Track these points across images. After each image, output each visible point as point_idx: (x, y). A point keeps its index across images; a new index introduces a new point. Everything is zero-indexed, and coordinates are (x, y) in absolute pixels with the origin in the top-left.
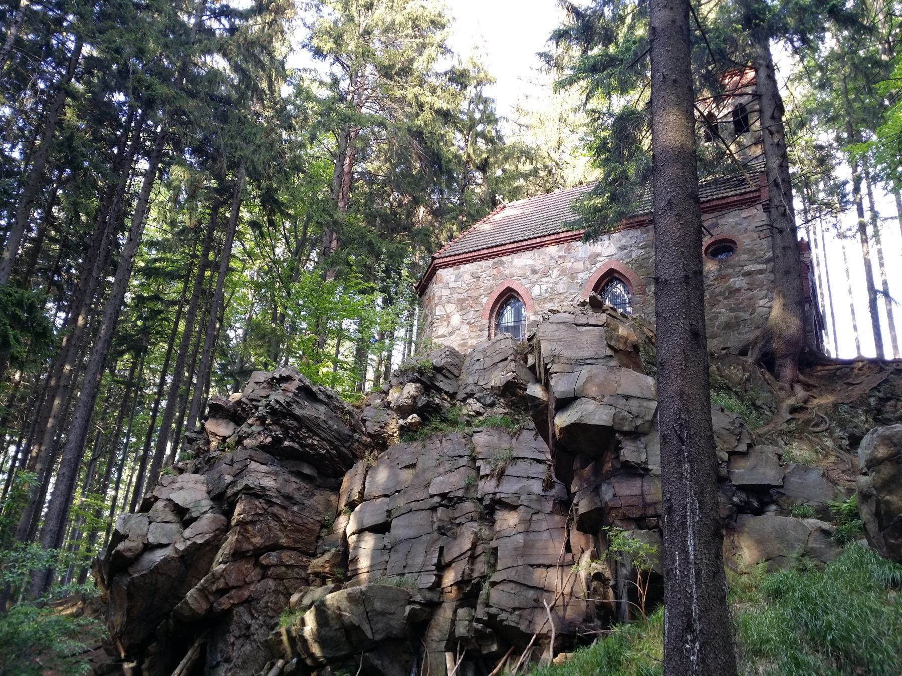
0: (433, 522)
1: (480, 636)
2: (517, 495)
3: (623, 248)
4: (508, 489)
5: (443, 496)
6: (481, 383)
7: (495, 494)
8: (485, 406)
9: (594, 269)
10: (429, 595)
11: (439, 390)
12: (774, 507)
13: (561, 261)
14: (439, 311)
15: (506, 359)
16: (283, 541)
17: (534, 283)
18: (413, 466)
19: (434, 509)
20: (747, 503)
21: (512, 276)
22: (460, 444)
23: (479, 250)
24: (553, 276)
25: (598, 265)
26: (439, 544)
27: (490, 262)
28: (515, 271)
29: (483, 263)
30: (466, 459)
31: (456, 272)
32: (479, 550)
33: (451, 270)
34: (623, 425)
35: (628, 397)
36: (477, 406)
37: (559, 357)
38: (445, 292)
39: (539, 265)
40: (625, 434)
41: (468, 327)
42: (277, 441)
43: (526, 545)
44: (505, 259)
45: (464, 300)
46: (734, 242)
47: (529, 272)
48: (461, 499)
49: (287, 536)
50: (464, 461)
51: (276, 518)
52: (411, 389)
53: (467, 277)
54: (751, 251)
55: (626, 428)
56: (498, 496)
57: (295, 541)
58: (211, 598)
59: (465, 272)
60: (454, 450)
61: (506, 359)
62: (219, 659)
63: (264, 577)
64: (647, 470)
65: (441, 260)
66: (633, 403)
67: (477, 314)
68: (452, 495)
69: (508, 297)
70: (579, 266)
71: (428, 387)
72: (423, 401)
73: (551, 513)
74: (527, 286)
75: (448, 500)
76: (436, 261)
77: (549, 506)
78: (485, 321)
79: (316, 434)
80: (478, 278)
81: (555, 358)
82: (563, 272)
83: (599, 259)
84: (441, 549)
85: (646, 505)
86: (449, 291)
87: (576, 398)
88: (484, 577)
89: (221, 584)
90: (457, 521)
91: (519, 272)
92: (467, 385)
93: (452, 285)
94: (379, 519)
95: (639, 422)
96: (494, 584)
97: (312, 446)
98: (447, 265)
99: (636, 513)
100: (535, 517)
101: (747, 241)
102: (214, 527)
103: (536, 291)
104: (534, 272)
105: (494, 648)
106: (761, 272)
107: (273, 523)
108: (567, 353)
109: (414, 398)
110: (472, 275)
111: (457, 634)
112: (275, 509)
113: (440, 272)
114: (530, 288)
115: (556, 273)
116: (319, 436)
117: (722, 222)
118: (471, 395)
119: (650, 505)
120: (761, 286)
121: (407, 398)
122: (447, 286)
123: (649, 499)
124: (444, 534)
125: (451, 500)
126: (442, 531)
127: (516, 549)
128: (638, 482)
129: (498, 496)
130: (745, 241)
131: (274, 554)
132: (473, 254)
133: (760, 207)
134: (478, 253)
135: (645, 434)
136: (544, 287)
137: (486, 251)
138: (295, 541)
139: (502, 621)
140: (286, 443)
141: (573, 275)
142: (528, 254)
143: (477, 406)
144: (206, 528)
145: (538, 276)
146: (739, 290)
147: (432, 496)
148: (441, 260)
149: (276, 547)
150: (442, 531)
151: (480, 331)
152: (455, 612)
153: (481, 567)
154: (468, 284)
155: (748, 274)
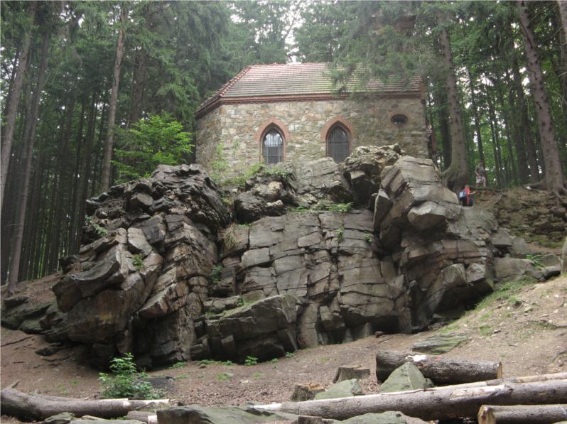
0: (302, 262)
1: (336, 319)
2: (353, 247)
3: (345, 110)
4: (346, 246)
5: (306, 248)
6: (314, 185)
7: (339, 247)
8: (317, 198)
9: (328, 120)
10: (304, 300)
11: (291, 187)
12: (508, 255)
13: (307, 112)
14: (224, 132)
15: (332, 173)
16: (199, 271)
17: (290, 123)
18: (281, 230)
19: (302, 255)
20: (498, 252)
21: (274, 116)
22: (312, 219)
23: (252, 97)
24: (302, 120)
25: (330, 118)
26: (307, 273)
27: (260, 106)
28: (277, 113)
29: (255, 105)
30: (317, 227)
31: (235, 108)
32: (333, 276)
33: (231, 106)
34: (448, 215)
35: (449, 202)
36: (313, 198)
37: (412, 179)
38: (228, 121)
39: (293, 111)
40: (448, 220)
41: (245, 145)
42: (195, 211)
43: (360, 274)
44: (269, 104)
45: (242, 127)
46: (406, 118)
47: (286, 115)
48: (317, 250)
49: (201, 268)
50: (316, 229)
51: (197, 257)
52: (277, 185)
53: (243, 112)
54: (415, 124)
55: (450, 217)
56: (341, 248)
57: (205, 271)
58: (170, 303)
59: (241, 109)
60: (308, 222)
61: (332, 173)
62: (169, 338)
63: (190, 291)
64: (460, 237)
65: (225, 99)
66: (451, 205)
67: (252, 137)
68: (312, 247)
69: (273, 129)
70: (318, 116)
71: (285, 185)
72: (284, 193)
73: (372, 258)
74: (286, 124)
75: (310, 250)
76: (221, 99)
77: (370, 254)
78: (257, 142)
79: (213, 208)
80: (251, 114)
81: (411, 179)
82: (309, 119)
83: (331, 114)
84: (309, 276)
85: (458, 253)
86: (230, 120)
87: (425, 201)
88: (337, 290)
89: (174, 295)
90: (317, 261)
91: (280, 114)
92: (304, 186)
93: (233, 116)
94: (267, 259)
95: (454, 215)
96: (343, 294)
97: (211, 215)
98: (229, 103)
99: (453, 256)
100: (364, 260)
101: (413, 118)
102: (157, 262)
103: (291, 127)
104: (290, 116)
105: (343, 325)
106: (420, 136)
107: (195, 261)
108: (416, 178)
109: (278, 191)
110: (247, 112)
111: (323, 319)
112: (197, 252)
113: (224, 107)
114: (288, 125)
115: (303, 119)
116: (215, 209)
117: (399, 104)
118: (308, 191)
119: (460, 253)
120: (420, 143)
121: (273, 190)
122: (229, 116)
123: (460, 250)
124: (309, 268)
125: (311, 250)
126: (308, 267)
127: (355, 276)
128: (455, 243)
129: (341, 248)
130: (411, 117)
131: (195, 278)
132: (248, 98)
133: (420, 100)
134: (251, 98)
135: (457, 220)
136: (297, 126)
137: (257, 98)
138: (205, 271)
139: (352, 311)
140: (200, 213)
141: (315, 121)
142: (287, 104)
143: (313, 198)
144: (153, 262)
145: (292, 119)
146: (409, 144)
147: (300, 248)
148: (225, 99)
149: (196, 275)
150: (308, 267)
151: (254, 148)
152: (319, 308)
153: (335, 285)
154: (244, 117)
155: (413, 136)
